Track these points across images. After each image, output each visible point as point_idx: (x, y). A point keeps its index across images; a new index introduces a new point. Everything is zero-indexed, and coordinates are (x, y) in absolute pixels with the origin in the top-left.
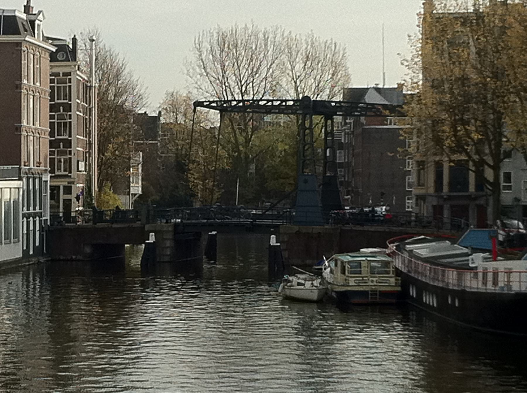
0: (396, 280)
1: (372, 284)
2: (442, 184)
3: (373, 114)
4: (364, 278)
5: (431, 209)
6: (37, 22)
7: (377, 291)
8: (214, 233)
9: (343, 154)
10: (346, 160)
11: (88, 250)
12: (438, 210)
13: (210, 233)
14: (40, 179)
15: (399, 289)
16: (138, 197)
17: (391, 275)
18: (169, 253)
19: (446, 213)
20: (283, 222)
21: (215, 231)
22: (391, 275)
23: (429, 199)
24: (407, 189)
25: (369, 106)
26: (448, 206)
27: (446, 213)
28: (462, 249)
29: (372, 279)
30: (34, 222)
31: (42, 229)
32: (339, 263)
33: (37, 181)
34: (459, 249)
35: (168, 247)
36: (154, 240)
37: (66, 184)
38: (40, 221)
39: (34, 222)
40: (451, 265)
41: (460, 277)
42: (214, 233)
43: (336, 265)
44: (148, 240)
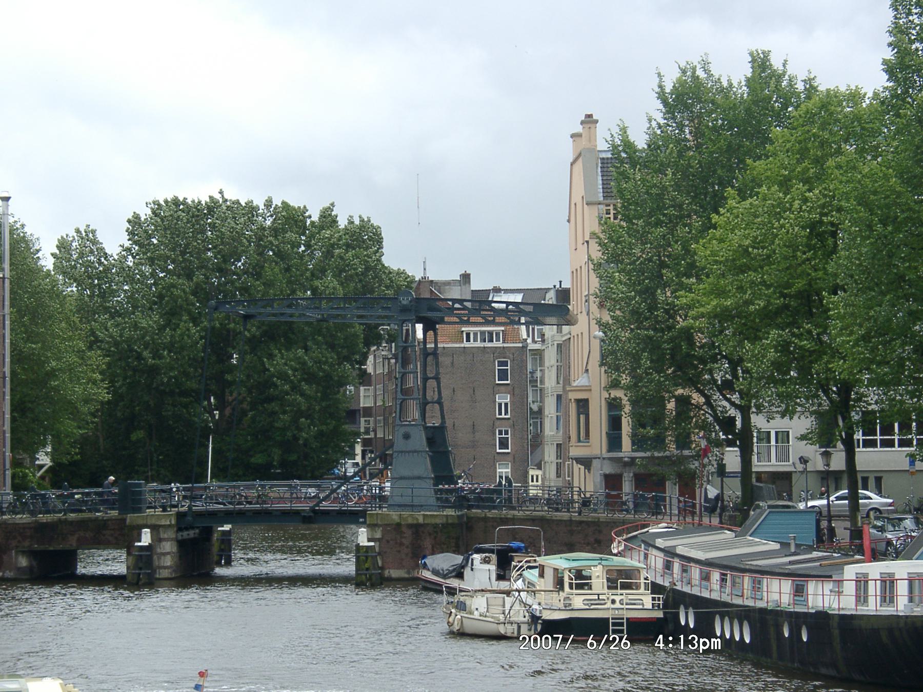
0: (654, 599)
1: (613, 606)
2: (620, 437)
3: (458, 320)
4: (601, 597)
5: (599, 479)
7: (623, 619)
8: (227, 527)
9: (371, 393)
10: (379, 403)
11: (23, 562)
12: (612, 481)
13: (219, 529)
15: (660, 614)
16: (46, 471)
17: (642, 590)
18: (169, 564)
19: (627, 487)
20: (371, 507)
21: (227, 523)
22: (642, 590)
23: (595, 463)
24: (498, 451)
25: (510, 307)
26: (631, 475)
27: (627, 487)
28: (764, 544)
29: (613, 597)
32: (549, 573)
34: (757, 544)
35: (168, 553)
36: (150, 542)
40: (777, 570)
41: (799, 591)
42: (227, 527)
43: (542, 575)
44: (140, 541)
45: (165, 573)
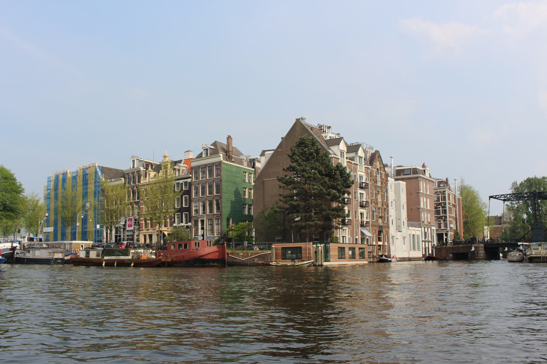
6: (426, 171)
11: (451, 255)
14: (431, 228)
30: (428, 245)
31: (432, 247)
33: (429, 229)
37: (446, 232)
38: (432, 244)
39: (428, 245)
45: (481, 258)
